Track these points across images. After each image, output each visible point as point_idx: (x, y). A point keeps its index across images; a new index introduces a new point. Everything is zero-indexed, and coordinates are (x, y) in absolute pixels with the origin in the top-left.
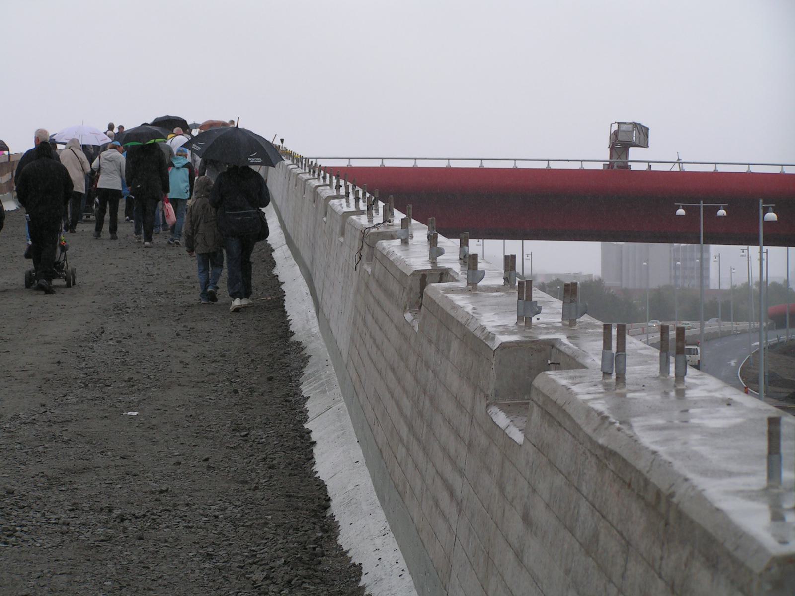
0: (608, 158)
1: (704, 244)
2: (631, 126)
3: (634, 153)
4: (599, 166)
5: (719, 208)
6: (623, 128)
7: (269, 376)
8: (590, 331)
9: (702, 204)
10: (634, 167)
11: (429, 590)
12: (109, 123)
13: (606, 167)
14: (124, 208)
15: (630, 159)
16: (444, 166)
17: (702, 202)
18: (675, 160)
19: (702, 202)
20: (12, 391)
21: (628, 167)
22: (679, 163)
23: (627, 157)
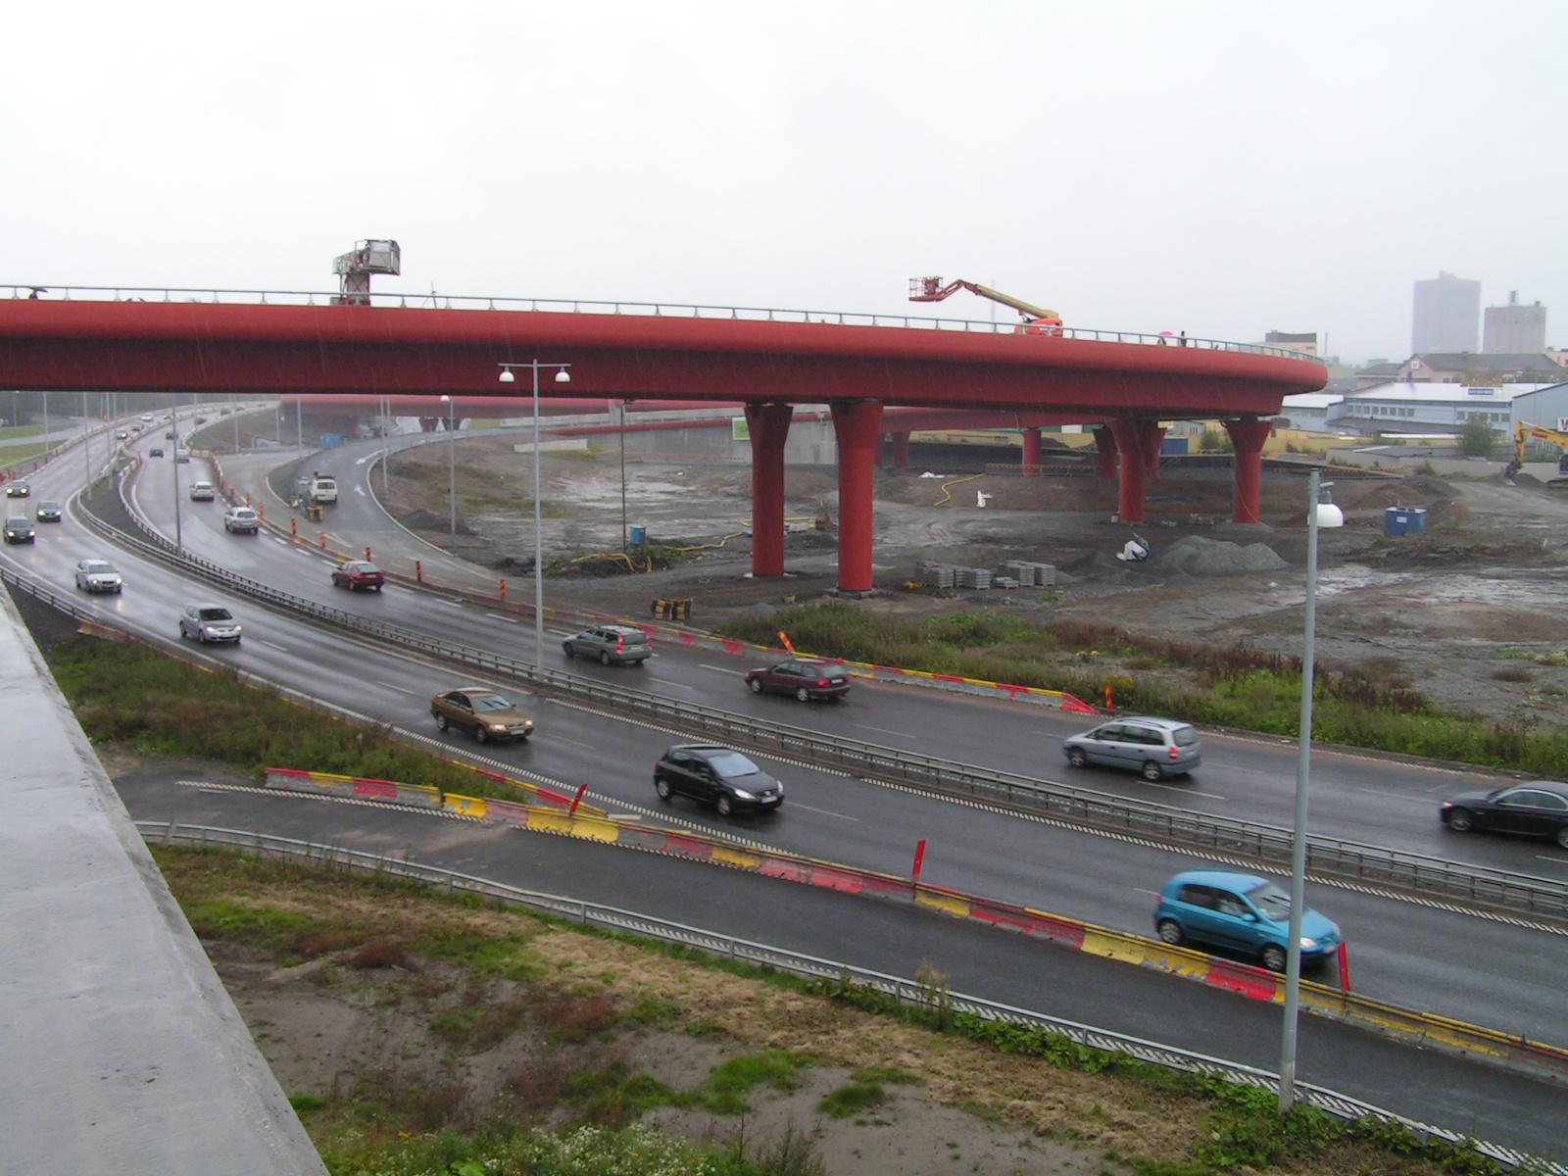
0: (338, 290)
1: (540, 415)
2: (387, 245)
3: (378, 282)
4: (324, 301)
5: (558, 370)
6: (377, 247)
7: (679, 751)
8: (206, 669)
9: (535, 365)
10: (375, 302)
11: (1172, 524)
12: (331, 267)
13: (337, 301)
14: (563, 448)
15: (371, 291)
16: (112, 299)
17: (535, 361)
18: (429, 293)
19: (535, 361)
20: (584, 1092)
21: (368, 302)
22: (434, 297)
23: (368, 288)
